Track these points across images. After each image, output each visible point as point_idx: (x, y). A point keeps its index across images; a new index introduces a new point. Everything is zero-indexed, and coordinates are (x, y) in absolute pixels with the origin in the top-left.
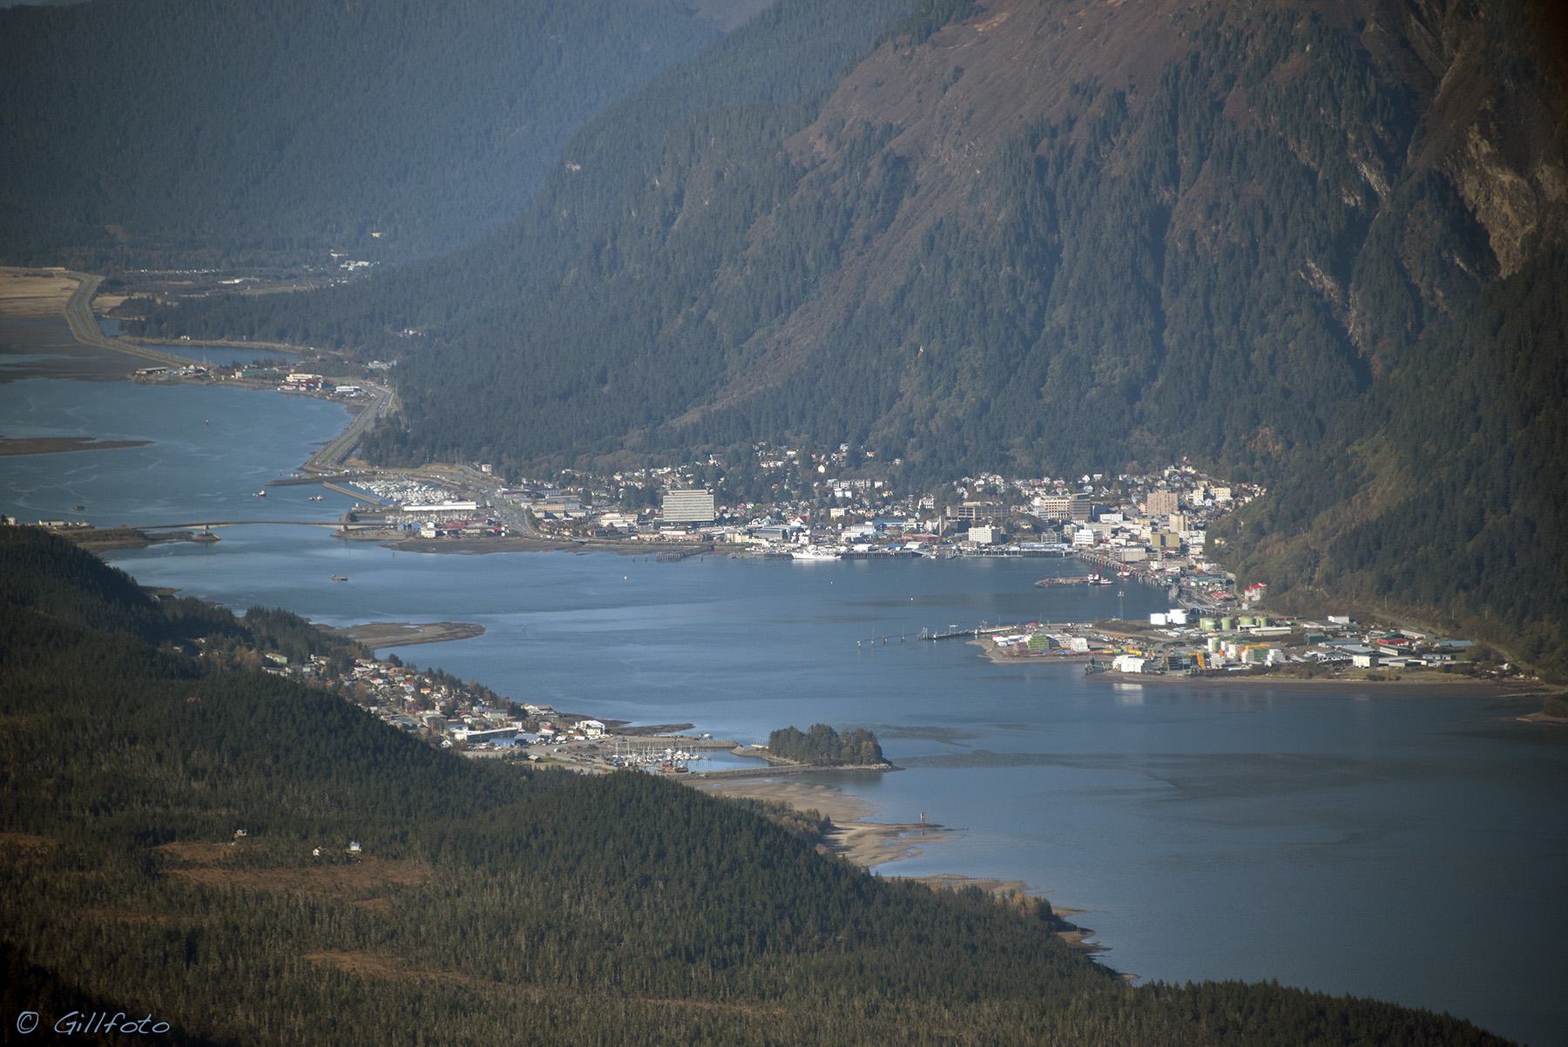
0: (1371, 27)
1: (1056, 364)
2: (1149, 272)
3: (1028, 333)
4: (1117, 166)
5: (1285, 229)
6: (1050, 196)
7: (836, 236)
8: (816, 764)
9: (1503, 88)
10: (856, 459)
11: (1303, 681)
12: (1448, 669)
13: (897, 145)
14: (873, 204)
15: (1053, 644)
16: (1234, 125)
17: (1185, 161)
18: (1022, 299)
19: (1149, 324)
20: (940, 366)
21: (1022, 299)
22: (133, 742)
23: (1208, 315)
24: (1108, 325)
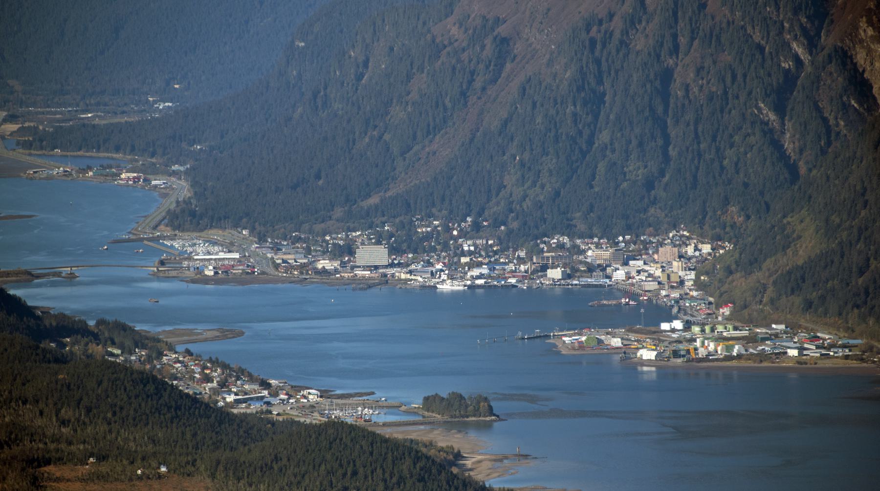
1: (602, 167)
2: (660, 110)
4: (640, 43)
5: (745, 82)
7: (464, 87)
8: (452, 417)
10: (477, 227)
11: (756, 365)
12: (847, 357)
13: (502, 30)
14: (487, 67)
15: (600, 342)
17: (683, 41)
18: (580, 126)
19: (660, 142)
20: (529, 168)
23: (696, 134)
24: (634, 142)
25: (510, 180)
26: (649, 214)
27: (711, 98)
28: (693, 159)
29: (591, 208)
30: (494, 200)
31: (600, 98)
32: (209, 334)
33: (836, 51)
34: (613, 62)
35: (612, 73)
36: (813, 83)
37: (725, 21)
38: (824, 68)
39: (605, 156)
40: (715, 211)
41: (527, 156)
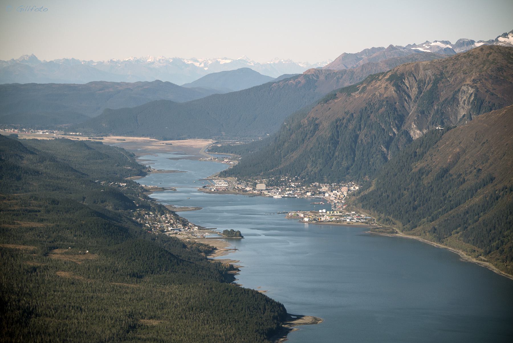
0: (397, 103)
1: (335, 162)
2: (354, 147)
3: (331, 157)
4: (351, 127)
5: (378, 139)
6: (338, 132)
7: (304, 138)
8: (228, 237)
9: (419, 116)
10: (297, 179)
11: (336, 224)
12: (362, 222)
13: (317, 122)
14: (311, 132)
15: (298, 215)
16: (371, 120)
17: (362, 126)
18: (331, 151)
19: (353, 156)
20: (314, 162)
21: (331, 151)
22: (68, 229)
23: (363, 154)
24: (345, 156)
25: (309, 165)
26: (346, 177)
27: (368, 144)
28: (361, 161)
29: (330, 175)
30: (304, 172)
31: (338, 143)
32: (191, 209)
33: (405, 131)
34: (342, 132)
35: (342, 135)
36: (397, 140)
37: (374, 121)
38: (401, 136)
39: (336, 160)
40: (362, 177)
41: (314, 159)
